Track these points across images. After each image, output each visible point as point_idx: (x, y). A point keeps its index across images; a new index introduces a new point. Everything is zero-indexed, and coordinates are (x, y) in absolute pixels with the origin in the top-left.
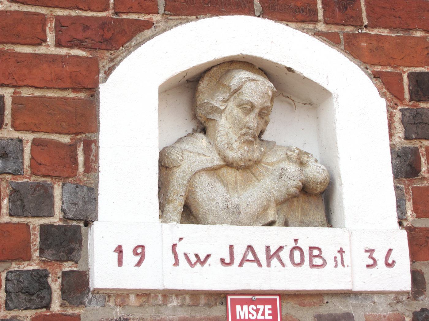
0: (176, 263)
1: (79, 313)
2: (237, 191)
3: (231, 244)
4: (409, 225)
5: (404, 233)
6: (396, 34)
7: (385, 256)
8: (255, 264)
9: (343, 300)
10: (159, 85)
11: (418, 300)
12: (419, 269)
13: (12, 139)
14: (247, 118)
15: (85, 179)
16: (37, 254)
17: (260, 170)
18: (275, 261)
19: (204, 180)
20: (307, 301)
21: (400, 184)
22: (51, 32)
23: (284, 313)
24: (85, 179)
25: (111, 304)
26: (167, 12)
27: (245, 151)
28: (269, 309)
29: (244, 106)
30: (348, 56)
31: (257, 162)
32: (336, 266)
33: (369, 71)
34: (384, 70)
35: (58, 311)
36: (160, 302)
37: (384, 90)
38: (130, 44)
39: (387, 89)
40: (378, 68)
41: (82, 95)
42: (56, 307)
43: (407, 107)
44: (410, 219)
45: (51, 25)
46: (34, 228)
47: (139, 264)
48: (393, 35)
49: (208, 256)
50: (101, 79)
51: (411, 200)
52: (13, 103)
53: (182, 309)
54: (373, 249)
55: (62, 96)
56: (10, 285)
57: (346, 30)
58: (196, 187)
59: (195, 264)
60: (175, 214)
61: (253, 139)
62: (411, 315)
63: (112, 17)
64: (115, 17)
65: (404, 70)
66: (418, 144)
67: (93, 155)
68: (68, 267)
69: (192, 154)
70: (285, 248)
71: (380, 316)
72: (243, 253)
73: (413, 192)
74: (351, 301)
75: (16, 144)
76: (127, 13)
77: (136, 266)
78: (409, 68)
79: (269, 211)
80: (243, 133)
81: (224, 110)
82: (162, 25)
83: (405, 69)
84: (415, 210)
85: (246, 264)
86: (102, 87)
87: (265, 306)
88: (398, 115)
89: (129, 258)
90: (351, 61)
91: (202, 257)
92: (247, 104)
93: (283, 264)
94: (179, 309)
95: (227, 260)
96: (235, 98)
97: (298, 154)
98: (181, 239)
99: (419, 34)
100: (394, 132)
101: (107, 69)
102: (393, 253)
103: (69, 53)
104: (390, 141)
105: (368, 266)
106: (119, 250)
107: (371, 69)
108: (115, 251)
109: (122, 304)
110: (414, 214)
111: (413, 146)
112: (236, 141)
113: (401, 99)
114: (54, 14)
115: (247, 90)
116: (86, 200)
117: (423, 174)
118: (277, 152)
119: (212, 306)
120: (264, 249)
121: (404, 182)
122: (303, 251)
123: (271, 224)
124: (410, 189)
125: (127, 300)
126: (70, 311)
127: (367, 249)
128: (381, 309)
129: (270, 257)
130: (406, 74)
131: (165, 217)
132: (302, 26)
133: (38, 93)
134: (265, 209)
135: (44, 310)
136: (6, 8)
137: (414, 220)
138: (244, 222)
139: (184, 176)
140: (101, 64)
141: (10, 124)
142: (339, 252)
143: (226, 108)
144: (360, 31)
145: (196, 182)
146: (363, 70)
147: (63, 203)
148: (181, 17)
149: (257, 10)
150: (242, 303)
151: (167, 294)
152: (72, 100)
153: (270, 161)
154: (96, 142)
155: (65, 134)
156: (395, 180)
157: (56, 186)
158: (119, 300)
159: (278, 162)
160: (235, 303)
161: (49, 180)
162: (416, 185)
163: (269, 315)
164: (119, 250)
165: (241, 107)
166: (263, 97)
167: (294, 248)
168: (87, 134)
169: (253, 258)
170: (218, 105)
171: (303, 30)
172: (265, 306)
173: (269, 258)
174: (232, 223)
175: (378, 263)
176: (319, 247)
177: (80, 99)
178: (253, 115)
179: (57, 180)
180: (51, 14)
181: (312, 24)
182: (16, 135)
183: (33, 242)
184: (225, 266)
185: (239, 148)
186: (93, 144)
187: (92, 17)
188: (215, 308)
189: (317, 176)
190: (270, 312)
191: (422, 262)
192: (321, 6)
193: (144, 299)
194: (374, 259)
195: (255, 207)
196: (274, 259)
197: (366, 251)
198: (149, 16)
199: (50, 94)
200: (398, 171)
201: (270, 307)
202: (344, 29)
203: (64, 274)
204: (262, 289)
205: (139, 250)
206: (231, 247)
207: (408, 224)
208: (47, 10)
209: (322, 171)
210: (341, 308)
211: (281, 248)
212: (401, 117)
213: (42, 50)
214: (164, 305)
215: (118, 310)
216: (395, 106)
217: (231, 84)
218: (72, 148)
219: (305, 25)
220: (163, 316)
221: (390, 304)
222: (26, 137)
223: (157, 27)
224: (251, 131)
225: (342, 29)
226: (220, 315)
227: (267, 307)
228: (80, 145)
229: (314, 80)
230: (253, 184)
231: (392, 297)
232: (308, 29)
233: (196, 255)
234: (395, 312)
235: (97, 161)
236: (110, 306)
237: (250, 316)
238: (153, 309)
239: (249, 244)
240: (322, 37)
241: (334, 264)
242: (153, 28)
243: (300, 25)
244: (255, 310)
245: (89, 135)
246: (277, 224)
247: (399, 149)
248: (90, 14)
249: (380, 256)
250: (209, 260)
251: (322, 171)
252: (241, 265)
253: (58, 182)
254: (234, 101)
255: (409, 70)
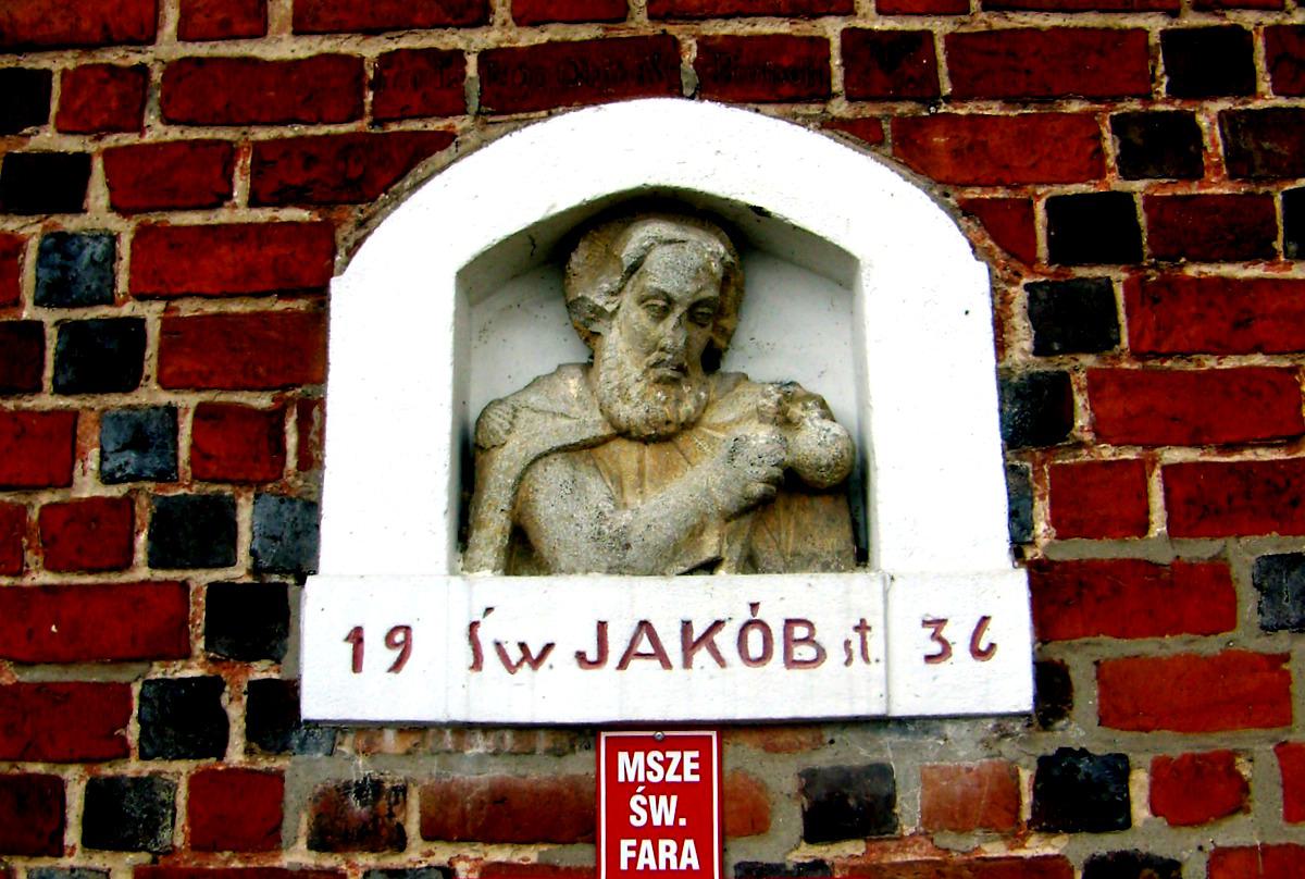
0: (477, 664)
1: (283, 768)
2: (641, 492)
3: (602, 620)
4: (1040, 555)
5: (1022, 575)
6: (1020, 111)
7: (970, 634)
8: (656, 663)
9: (869, 734)
10: (457, 269)
11: (1052, 731)
12: (1057, 658)
13: (156, 408)
14: (661, 327)
15: (300, 483)
16: (201, 644)
17: (695, 441)
18: (702, 656)
19: (555, 474)
20: (783, 738)
21: (1021, 460)
22: (244, 178)
23: (728, 766)
24: (300, 483)
25: (346, 749)
26: (483, 109)
27: (657, 401)
28: (693, 760)
29: (650, 302)
30: (901, 170)
31: (689, 425)
32: (848, 662)
33: (952, 201)
34: (987, 197)
35: (241, 762)
36: (450, 746)
37: (988, 242)
38: (402, 187)
39: (993, 238)
40: (973, 193)
41: (301, 305)
42: (236, 755)
43: (1043, 279)
44: (1042, 541)
45: (244, 162)
46: (198, 591)
47: (397, 666)
48: (1012, 114)
49: (549, 647)
50: (337, 266)
51: (1047, 497)
52: (163, 332)
53: (498, 760)
54: (942, 617)
55: (259, 309)
56: (146, 710)
57: (899, 111)
58: (537, 490)
59: (519, 664)
60: (491, 550)
61: (675, 375)
62: (1035, 765)
63: (368, 130)
64: (377, 130)
65: (1039, 193)
66: (1066, 364)
67: (315, 433)
68: (261, 671)
69: (539, 416)
70: (727, 623)
71: (959, 767)
72: (630, 638)
73: (1051, 479)
74: (889, 737)
75: (162, 418)
76: (399, 120)
77: (390, 670)
78: (1050, 188)
79: (706, 537)
80: (651, 363)
81: (614, 314)
82: (472, 138)
83: (1040, 191)
84: (1055, 521)
85: (634, 663)
86: (336, 284)
87: (685, 753)
88: (1019, 296)
89: (378, 654)
90: (907, 180)
91: (535, 652)
92: (656, 297)
93: (721, 661)
94: (492, 760)
95: (592, 656)
96: (634, 286)
97: (779, 403)
98: (489, 610)
99: (1075, 107)
100: (1013, 338)
101: (351, 244)
102: (991, 624)
103: (276, 218)
104: (998, 361)
105: (929, 658)
106: (356, 637)
107: (956, 194)
108: (347, 639)
109: (369, 749)
110: (1052, 529)
111: (1055, 369)
112: (638, 381)
113: (1030, 261)
114: (251, 138)
115: (655, 266)
116: (300, 528)
117: (1078, 434)
118: (741, 398)
119: (564, 754)
120: (678, 628)
121: (1033, 454)
122: (770, 631)
123: (710, 566)
124: (1046, 470)
125: (377, 740)
126: (263, 764)
127: (929, 619)
128: (962, 754)
129: (691, 645)
130: (1044, 200)
131: (471, 559)
132: (793, 109)
133: (212, 308)
134: (695, 532)
135: (213, 760)
136: (159, 136)
137: (1050, 545)
138: (640, 564)
139: (509, 468)
140: (340, 235)
141: (154, 376)
142: (857, 628)
143: (618, 308)
144: (932, 109)
145: (535, 479)
146: (934, 199)
147: (254, 537)
148: (514, 116)
149: (686, 83)
150: (632, 746)
151: (463, 729)
152: (279, 317)
153: (719, 421)
154: (322, 403)
155: (263, 390)
156: (1008, 454)
157: (242, 501)
158: (361, 742)
159: (737, 422)
160: (614, 747)
161: (228, 490)
162: (1059, 462)
163: (693, 772)
164: (356, 637)
165: (645, 304)
166: (696, 279)
167: (749, 624)
168: (304, 388)
169: (651, 650)
170: (600, 302)
171: (796, 118)
172: (685, 753)
173: (689, 647)
174: (611, 570)
175: (954, 650)
176: (809, 619)
177: (297, 313)
178: (671, 321)
179: (245, 488)
180: (247, 139)
181: (814, 103)
182: (165, 398)
183: (194, 620)
184: (587, 668)
185: (643, 398)
186: (316, 408)
187: (327, 136)
188: (570, 758)
189: (819, 451)
190: (696, 766)
191: (1067, 642)
192: (838, 62)
193: (414, 739)
194: (943, 642)
195: (666, 530)
196: (700, 649)
197: (926, 623)
198: (447, 122)
199: (235, 307)
200: (1015, 433)
201: (696, 754)
202: (894, 109)
203: (251, 684)
204: (668, 719)
205: (399, 637)
206: (602, 626)
207: (1036, 555)
208: (238, 130)
209: (832, 439)
210: (864, 752)
211: (718, 624)
212: (1026, 302)
213: (222, 216)
214: (457, 751)
215: (360, 762)
216: (1016, 278)
217: (622, 256)
218: (275, 419)
219: (800, 109)
220: (457, 775)
221: (982, 741)
222: (183, 401)
223: (461, 142)
224: (669, 357)
225: (887, 109)
226: (582, 772)
227: (688, 755)
228: (292, 412)
229: (815, 231)
230: (679, 474)
231: (990, 726)
232: (805, 116)
233: (523, 646)
234: (996, 760)
235: (321, 445)
236: (343, 753)
237: (650, 774)
238: (435, 760)
239: (643, 619)
240: (840, 132)
241: (845, 658)
242: (453, 147)
243: (787, 108)
244: (660, 763)
245: (308, 389)
246: (725, 565)
247: (1022, 379)
248: (322, 130)
249: (959, 635)
250: (551, 657)
251: (832, 439)
252: (623, 664)
253: (247, 491)
254: (632, 290)
255: (1050, 191)
